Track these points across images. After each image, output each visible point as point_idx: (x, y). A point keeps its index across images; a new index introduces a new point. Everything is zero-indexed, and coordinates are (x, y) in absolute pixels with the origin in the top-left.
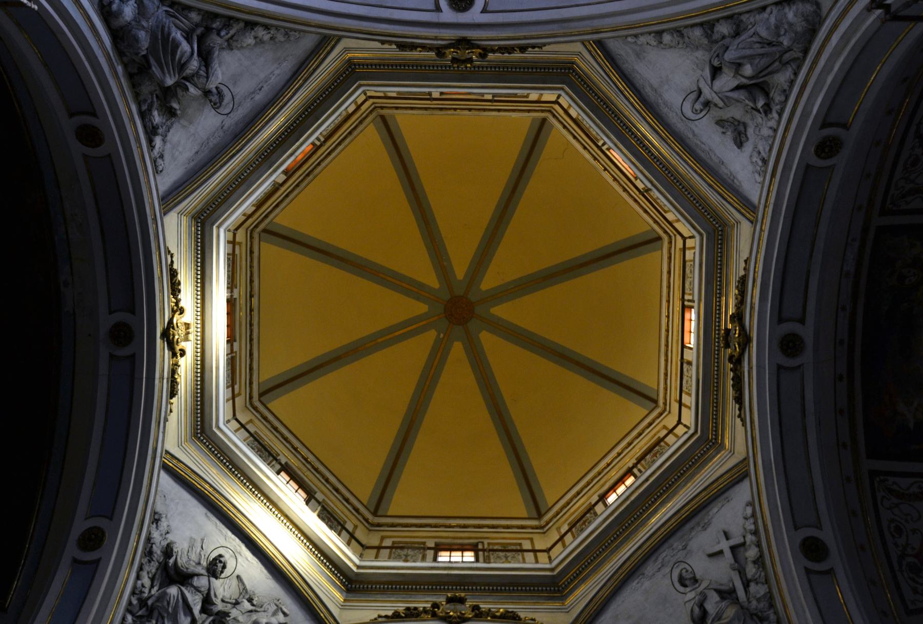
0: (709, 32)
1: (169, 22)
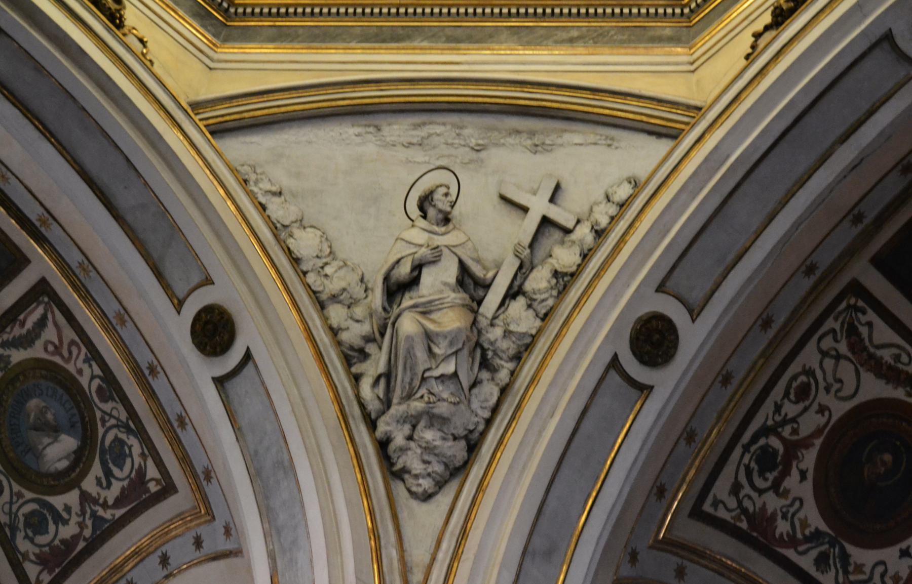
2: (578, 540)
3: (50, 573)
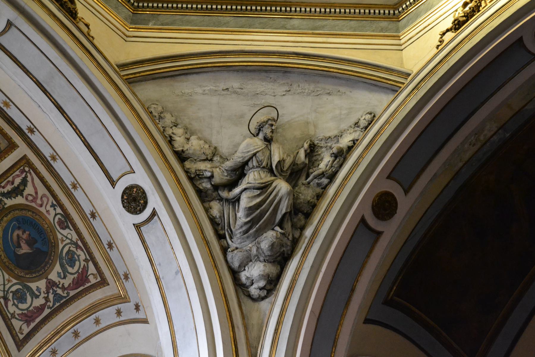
1: (236, 230)
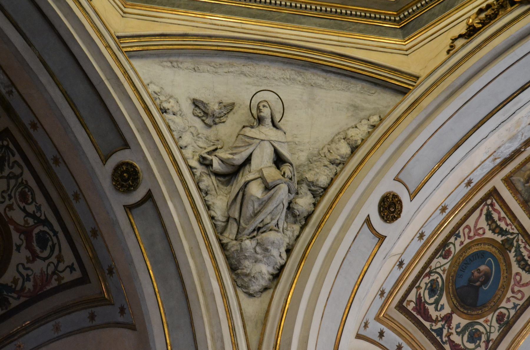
0: (313, 188)
2: (400, 328)
3: (414, 309)
